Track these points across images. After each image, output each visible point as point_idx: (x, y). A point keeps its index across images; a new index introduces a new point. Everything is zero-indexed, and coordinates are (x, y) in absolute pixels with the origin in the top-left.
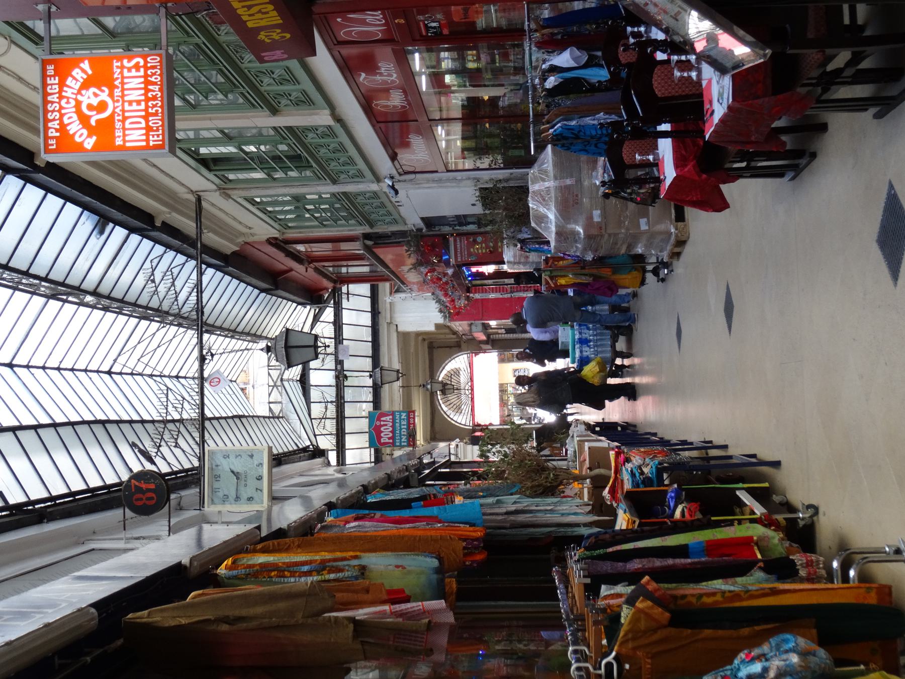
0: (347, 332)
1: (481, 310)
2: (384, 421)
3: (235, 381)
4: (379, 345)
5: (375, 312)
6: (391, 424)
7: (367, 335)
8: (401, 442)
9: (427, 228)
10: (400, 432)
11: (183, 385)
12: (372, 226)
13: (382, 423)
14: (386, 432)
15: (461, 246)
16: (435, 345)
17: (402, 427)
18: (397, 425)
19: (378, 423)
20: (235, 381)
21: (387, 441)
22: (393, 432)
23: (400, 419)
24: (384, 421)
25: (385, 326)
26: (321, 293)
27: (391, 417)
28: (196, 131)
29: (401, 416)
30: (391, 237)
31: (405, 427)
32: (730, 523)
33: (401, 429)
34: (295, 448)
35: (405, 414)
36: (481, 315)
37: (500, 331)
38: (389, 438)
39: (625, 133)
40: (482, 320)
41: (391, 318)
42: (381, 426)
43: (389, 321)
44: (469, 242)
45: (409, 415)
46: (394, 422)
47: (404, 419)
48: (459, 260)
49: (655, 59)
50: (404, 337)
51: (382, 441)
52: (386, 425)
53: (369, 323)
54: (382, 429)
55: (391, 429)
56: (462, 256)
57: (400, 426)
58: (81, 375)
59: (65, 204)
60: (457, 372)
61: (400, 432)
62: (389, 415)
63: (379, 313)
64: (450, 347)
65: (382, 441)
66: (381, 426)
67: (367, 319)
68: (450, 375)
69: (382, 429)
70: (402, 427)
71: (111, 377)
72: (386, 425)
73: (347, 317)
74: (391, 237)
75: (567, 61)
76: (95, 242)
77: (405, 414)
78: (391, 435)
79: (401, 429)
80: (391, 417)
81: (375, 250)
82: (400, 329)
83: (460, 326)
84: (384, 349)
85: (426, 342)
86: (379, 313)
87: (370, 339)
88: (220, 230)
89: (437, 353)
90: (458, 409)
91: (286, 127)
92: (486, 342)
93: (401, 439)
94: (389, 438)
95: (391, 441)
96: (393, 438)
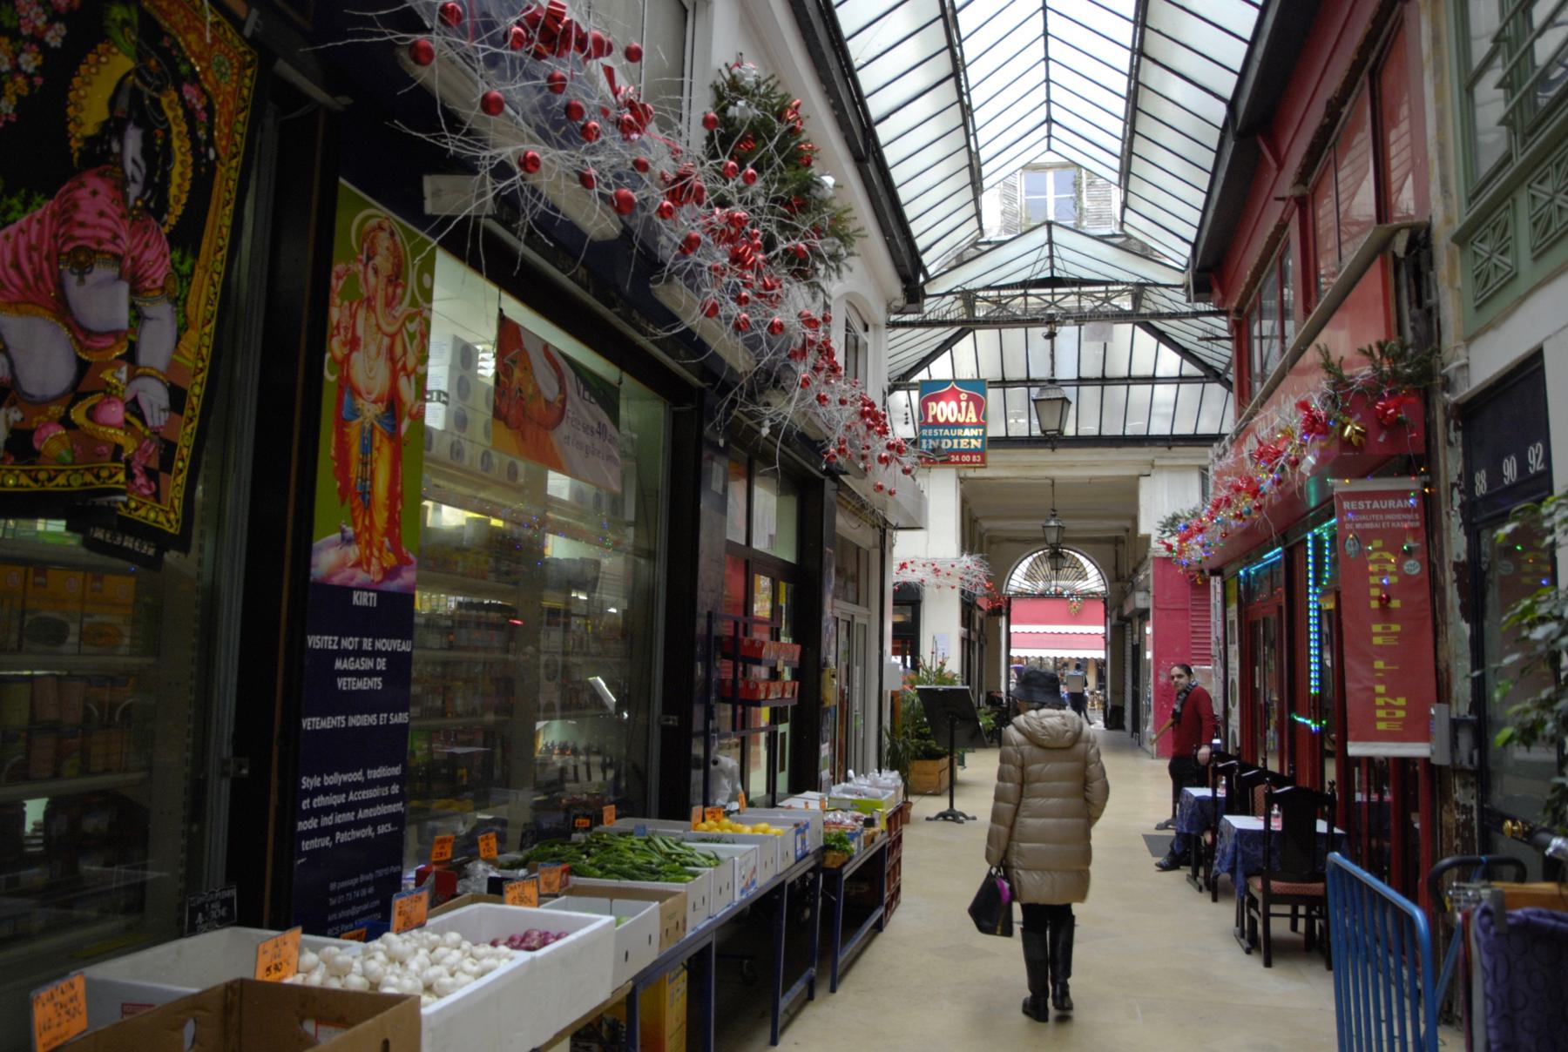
0: (1140, 392)
1: (1172, 606)
2: (967, 407)
3: (1049, 149)
4: (1118, 446)
5: (1171, 441)
6: (961, 420)
7: (1135, 427)
8: (927, 438)
9: (1456, 405)
10: (947, 437)
12: (1463, 239)
13: (964, 404)
14: (947, 412)
15: (1389, 511)
16: (1120, 547)
19: (963, 397)
20: (1049, 149)
21: (931, 413)
24: (967, 407)
25: (1149, 458)
26: (1217, 291)
27: (974, 420)
30: (1419, 304)
31: (955, 446)
33: (951, 438)
34: (876, 107)
35: (979, 445)
36: (1162, 606)
37: (1136, 637)
40: (1155, 607)
41: (1162, 466)
42: (959, 401)
44: (1401, 535)
47: (969, 443)
48: (1346, 505)
49: (67, 26)
52: (960, 411)
53: (1154, 431)
55: (952, 420)
56: (1355, 512)
58: (1037, 51)
60: (1082, 576)
63: (1170, 448)
64: (1116, 567)
66: (959, 401)
67: (1160, 427)
68: (1077, 565)
70: (956, 441)
72: (960, 411)
73: (1164, 393)
74: (1419, 304)
77: (979, 445)
79: (951, 438)
81: (1375, 271)
82: (1143, 481)
83: (1148, 575)
84: (1112, 454)
85: (1123, 534)
86: (1170, 448)
87: (1128, 432)
89: (1110, 548)
90: (1030, 576)
92: (1120, 618)
94: (935, 417)
95: (930, 420)
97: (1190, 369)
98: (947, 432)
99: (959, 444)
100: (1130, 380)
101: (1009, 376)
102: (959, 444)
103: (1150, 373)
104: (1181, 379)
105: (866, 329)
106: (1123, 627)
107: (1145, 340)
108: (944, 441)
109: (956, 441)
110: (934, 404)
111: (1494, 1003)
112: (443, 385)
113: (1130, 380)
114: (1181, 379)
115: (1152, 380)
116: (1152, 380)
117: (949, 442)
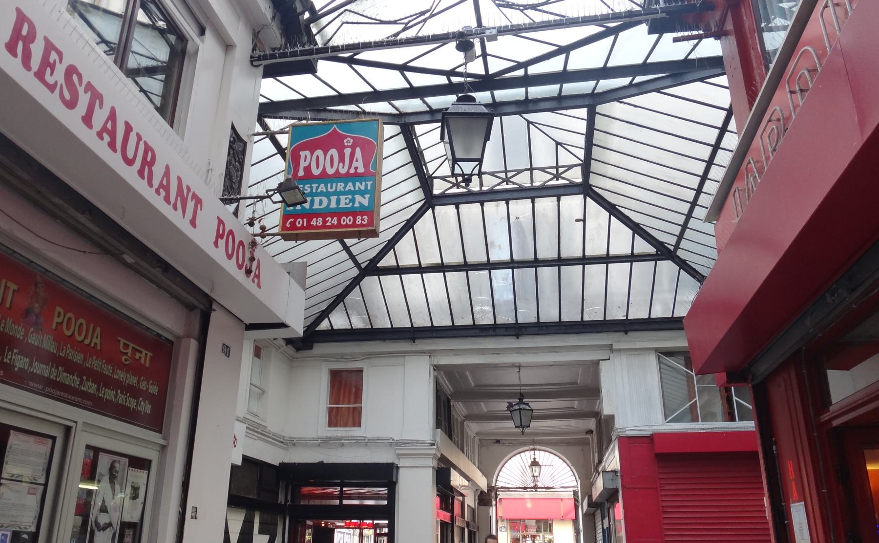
0: (595, 271)
5: (627, 326)
10: (322, 194)
13: (347, 151)
17: (334, 199)
18: (340, 186)
19: (348, 142)
21: (303, 164)
22: (324, 175)
23: (353, 193)
27: (361, 170)
28: (536, 491)
29: (362, 193)
31: (333, 205)
33: (328, 195)
35: (365, 202)
38: (308, 169)
40: (623, 486)
41: (619, 350)
43: (614, 347)
45: (362, 213)
46: (355, 176)
47: (353, 201)
50: (596, 364)
51: (303, 154)
54: (333, 152)
55: (330, 171)
61: (322, 194)
62: (366, 165)
69: (333, 152)
71: (522, 117)
72: (342, 159)
73: (618, 270)
75: (327, 327)
77: (365, 202)
78: (316, 172)
80: (361, 170)
82: (603, 364)
86: (626, 333)
94: (308, 169)
95: (301, 173)
96: (309, 176)
97: (643, 247)
98: (322, 187)
99: (338, 202)
100: (584, 260)
101: (470, 259)
102: (338, 202)
103: (603, 252)
104: (632, 258)
105: (202, 32)
106: (594, 515)
107: (598, 215)
108: (317, 199)
110: (308, 153)
111: (158, 267)
112: (344, 503)
113: (584, 260)
114: (632, 258)
115: (607, 259)
116: (607, 259)
117: (325, 200)
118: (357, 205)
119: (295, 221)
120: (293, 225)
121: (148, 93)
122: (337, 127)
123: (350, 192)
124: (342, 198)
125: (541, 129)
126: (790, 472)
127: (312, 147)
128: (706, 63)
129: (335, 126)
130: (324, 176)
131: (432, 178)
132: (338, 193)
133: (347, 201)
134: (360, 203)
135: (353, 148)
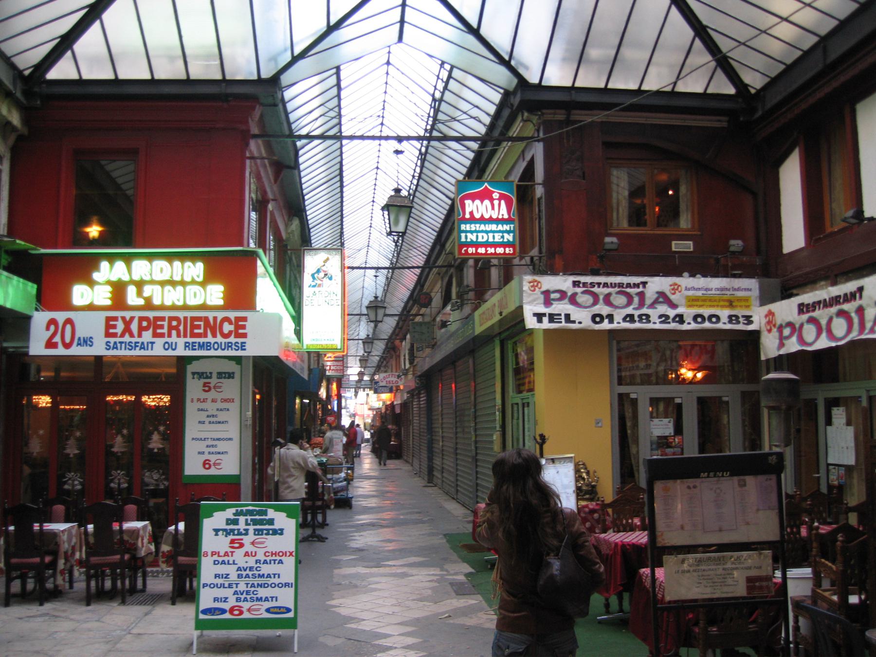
2: (499, 205)
6: (495, 217)
10: (482, 231)
11: (455, 150)
13: (496, 202)
18: (483, 227)
19: (496, 196)
21: (468, 210)
24: (499, 205)
27: (506, 216)
31: (491, 240)
32: (349, 521)
39: (826, 547)
42: (492, 200)
47: (503, 237)
51: (468, 202)
52: (493, 208)
55: (487, 216)
57: (491, 231)
59: (462, 174)
61: (482, 231)
65: (468, 202)
66: (492, 200)
72: (493, 208)
76: (453, 181)
79: (487, 232)
88: (707, 39)
91: (39, 311)
93: (471, 232)
94: (471, 213)
95: (467, 216)
99: (494, 237)
102: (494, 237)
109: (491, 235)
118: (469, 240)
119: (467, 249)
120: (466, 251)
121: (312, 134)
122: (490, 186)
123: (500, 231)
124: (496, 235)
125: (320, 50)
126: (713, 567)
127: (473, 197)
128: (792, 646)
129: (486, 184)
130: (482, 220)
131: (498, 218)
132: (494, 232)
133: (500, 237)
134: (507, 239)
135: (500, 199)
